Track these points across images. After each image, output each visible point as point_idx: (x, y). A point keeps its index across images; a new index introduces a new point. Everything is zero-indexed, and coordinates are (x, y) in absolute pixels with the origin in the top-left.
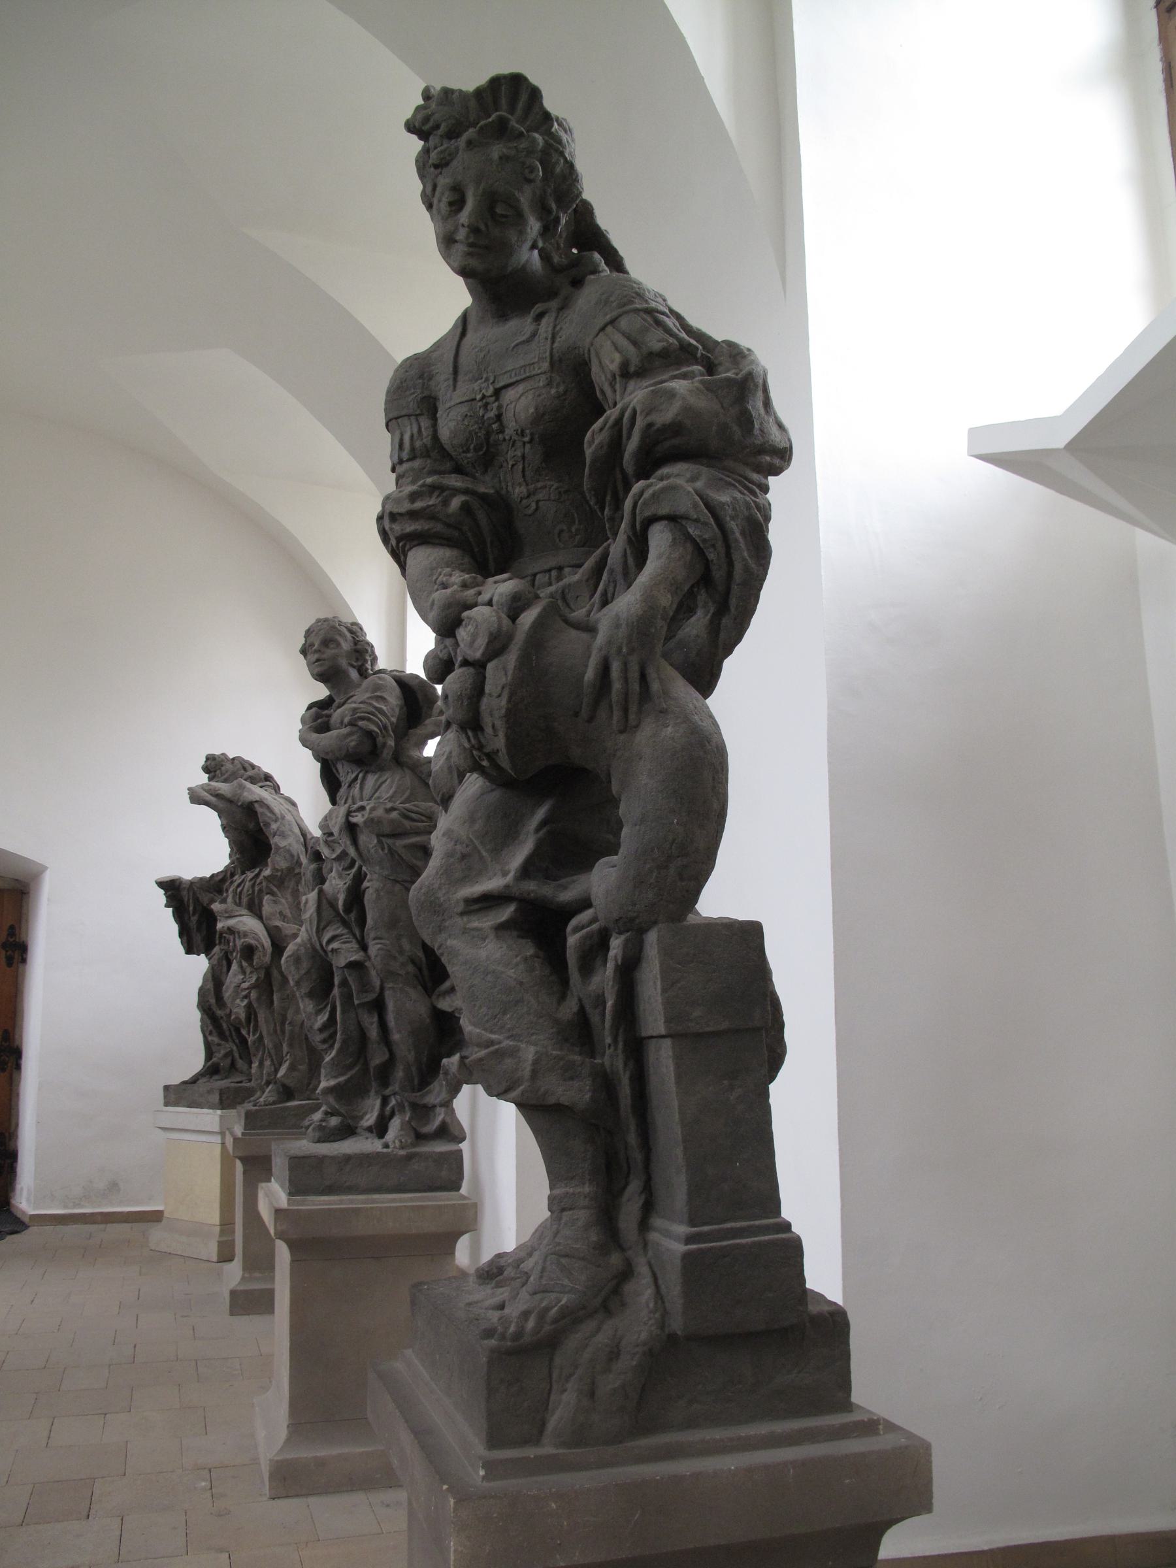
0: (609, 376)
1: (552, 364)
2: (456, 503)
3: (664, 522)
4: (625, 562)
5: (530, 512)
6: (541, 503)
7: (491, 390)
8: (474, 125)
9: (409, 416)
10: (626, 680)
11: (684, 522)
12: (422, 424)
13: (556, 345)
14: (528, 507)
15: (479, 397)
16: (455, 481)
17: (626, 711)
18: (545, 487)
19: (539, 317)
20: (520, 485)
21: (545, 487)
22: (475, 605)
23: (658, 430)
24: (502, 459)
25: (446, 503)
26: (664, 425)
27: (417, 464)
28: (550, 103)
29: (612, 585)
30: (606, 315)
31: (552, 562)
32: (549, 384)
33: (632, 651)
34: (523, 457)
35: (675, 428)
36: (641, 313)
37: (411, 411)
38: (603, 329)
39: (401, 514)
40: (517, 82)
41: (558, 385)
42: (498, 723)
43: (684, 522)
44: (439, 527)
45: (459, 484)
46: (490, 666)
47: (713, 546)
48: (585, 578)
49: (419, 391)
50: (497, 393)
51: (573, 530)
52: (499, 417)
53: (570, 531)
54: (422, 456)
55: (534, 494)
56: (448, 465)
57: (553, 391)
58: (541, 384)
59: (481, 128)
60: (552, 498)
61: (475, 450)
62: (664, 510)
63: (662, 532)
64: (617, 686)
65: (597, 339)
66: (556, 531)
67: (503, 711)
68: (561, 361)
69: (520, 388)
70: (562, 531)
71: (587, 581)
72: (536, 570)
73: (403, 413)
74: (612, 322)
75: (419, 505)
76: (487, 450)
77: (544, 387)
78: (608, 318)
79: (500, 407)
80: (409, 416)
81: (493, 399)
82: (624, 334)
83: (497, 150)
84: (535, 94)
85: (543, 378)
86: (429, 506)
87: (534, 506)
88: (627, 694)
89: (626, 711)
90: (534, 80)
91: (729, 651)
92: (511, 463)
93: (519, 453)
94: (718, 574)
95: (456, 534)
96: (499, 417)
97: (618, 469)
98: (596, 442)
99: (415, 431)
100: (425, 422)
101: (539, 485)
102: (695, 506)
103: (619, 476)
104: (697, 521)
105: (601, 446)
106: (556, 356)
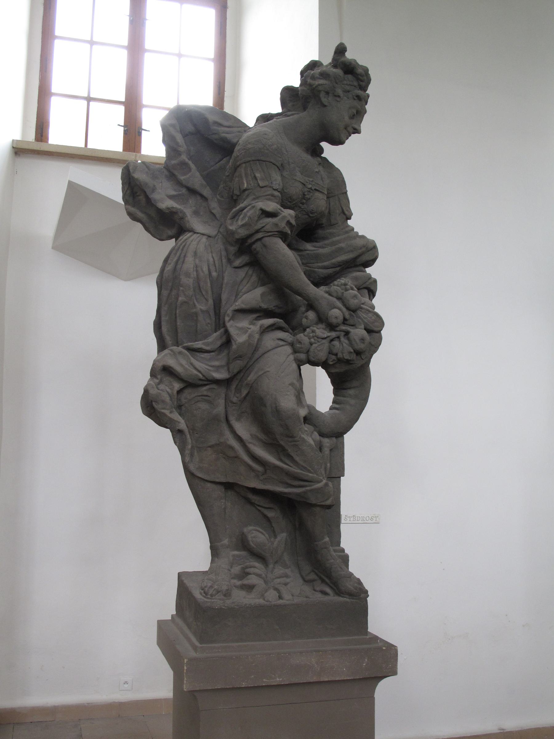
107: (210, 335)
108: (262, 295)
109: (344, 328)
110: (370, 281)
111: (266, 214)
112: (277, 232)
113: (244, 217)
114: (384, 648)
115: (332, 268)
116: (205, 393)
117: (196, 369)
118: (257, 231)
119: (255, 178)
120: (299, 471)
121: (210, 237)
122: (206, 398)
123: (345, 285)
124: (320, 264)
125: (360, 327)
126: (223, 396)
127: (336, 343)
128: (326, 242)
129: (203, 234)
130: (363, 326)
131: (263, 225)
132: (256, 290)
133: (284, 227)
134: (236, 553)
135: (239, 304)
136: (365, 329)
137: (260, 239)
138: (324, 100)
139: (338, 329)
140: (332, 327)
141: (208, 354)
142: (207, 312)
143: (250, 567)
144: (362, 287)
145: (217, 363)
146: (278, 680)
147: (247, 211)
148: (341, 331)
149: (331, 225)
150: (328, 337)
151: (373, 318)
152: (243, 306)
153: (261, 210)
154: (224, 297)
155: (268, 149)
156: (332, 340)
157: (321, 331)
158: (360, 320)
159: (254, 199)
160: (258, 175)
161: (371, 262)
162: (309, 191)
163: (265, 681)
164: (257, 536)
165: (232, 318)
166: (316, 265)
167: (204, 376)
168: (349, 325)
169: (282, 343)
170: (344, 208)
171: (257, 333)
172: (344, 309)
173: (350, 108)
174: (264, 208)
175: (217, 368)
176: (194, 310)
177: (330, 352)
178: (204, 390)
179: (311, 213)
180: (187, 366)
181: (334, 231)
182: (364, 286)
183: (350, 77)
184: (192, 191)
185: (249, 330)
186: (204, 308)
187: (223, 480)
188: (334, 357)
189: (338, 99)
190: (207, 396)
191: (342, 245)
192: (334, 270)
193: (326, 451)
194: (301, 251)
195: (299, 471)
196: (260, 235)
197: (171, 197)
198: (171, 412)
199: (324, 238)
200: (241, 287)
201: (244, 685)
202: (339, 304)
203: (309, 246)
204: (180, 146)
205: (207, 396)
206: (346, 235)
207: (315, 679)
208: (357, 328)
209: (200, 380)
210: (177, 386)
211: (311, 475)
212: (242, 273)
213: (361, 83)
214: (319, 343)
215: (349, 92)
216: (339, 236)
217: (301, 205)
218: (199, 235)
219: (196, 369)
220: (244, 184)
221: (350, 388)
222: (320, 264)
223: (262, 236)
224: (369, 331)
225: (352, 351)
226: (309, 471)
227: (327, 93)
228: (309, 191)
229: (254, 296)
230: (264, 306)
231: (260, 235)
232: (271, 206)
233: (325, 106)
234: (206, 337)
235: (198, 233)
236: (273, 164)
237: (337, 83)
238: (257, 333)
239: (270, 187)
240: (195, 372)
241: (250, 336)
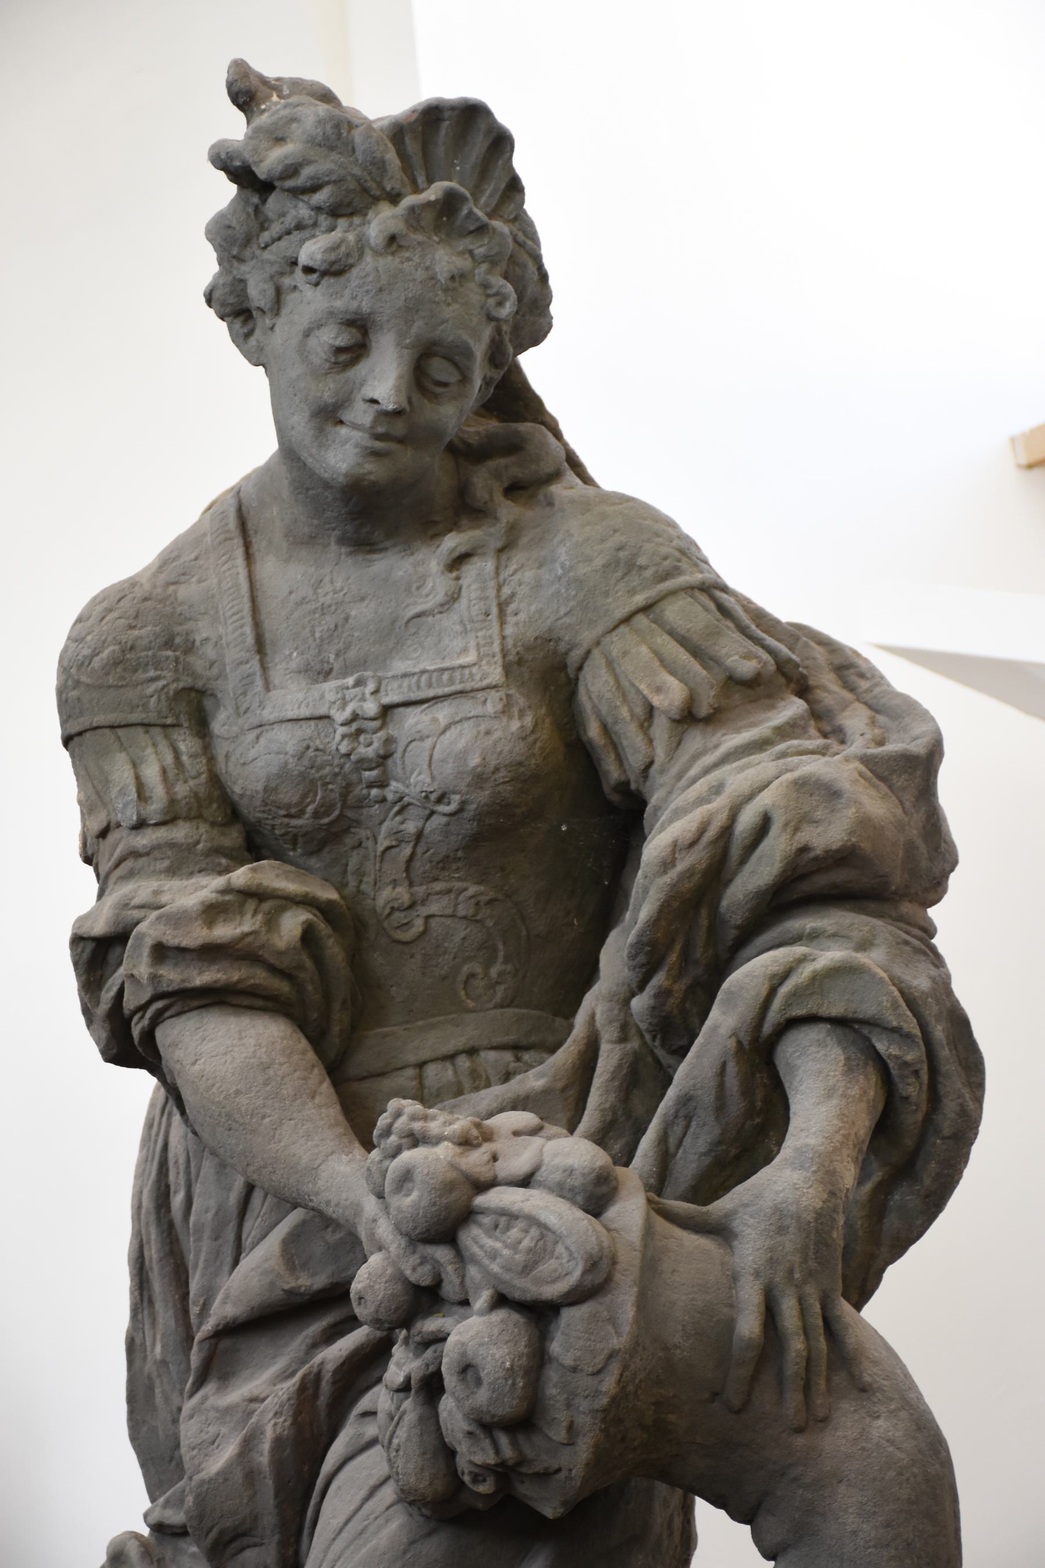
0: (639, 710)
1: (507, 669)
2: (292, 924)
3: (826, 1027)
4: (721, 1086)
5: (400, 935)
6: (433, 922)
7: (371, 708)
8: (394, 198)
9: (146, 726)
10: (806, 1331)
11: (865, 1031)
12: (182, 747)
13: (509, 630)
14: (408, 925)
15: (340, 716)
16: (270, 875)
17: (807, 1389)
18: (449, 891)
19: (458, 561)
20: (395, 883)
21: (449, 891)
22: (493, 1183)
23: (816, 859)
24: (363, 833)
25: (271, 922)
26: (827, 852)
27: (180, 833)
28: (521, 162)
29: (681, 1122)
30: (632, 592)
31: (457, 1041)
32: (506, 710)
33: (811, 1274)
34: (419, 835)
35: (844, 857)
36: (697, 593)
37: (152, 717)
38: (627, 620)
39: (182, 950)
40: (472, 113)
41: (521, 715)
42: (583, 1420)
43: (865, 1031)
44: (260, 977)
45: (291, 886)
46: (570, 1316)
47: (916, 1073)
48: (560, 1085)
49: (169, 675)
50: (386, 711)
51: (494, 972)
52: (384, 758)
53: (486, 974)
54: (188, 818)
55: (424, 902)
56: (233, 838)
57: (515, 725)
58: (490, 709)
59: (412, 210)
60: (461, 911)
61: (316, 815)
62: (836, 1008)
63: (821, 1044)
64: (796, 1345)
65: (614, 637)
66: (462, 977)
67: (605, 1401)
68: (520, 662)
69: (443, 713)
70: (472, 976)
71: (564, 1090)
72: (425, 1054)
73: (135, 717)
74: (646, 609)
75: (224, 931)
76: (341, 815)
77: (496, 717)
78: (640, 599)
79: (389, 741)
80: (146, 726)
81: (376, 724)
82: (672, 633)
83: (445, 259)
84: (501, 142)
85: (494, 695)
86: (246, 935)
87: (419, 925)
88: (809, 1360)
89: (807, 1389)
90: (503, 116)
91: (899, 1249)
92: (383, 843)
93: (411, 827)
94: (912, 1119)
95: (283, 987)
96: (384, 758)
97: (704, 912)
98: (680, 867)
99: (169, 759)
100: (187, 744)
101: (438, 886)
102: (895, 1006)
103: (704, 922)
104: (895, 1030)
105: (689, 873)
106: (512, 657)
173: (307, 334)
182: (774, 1016)
217: (374, 792)
228: (359, 732)
237: (240, 259)
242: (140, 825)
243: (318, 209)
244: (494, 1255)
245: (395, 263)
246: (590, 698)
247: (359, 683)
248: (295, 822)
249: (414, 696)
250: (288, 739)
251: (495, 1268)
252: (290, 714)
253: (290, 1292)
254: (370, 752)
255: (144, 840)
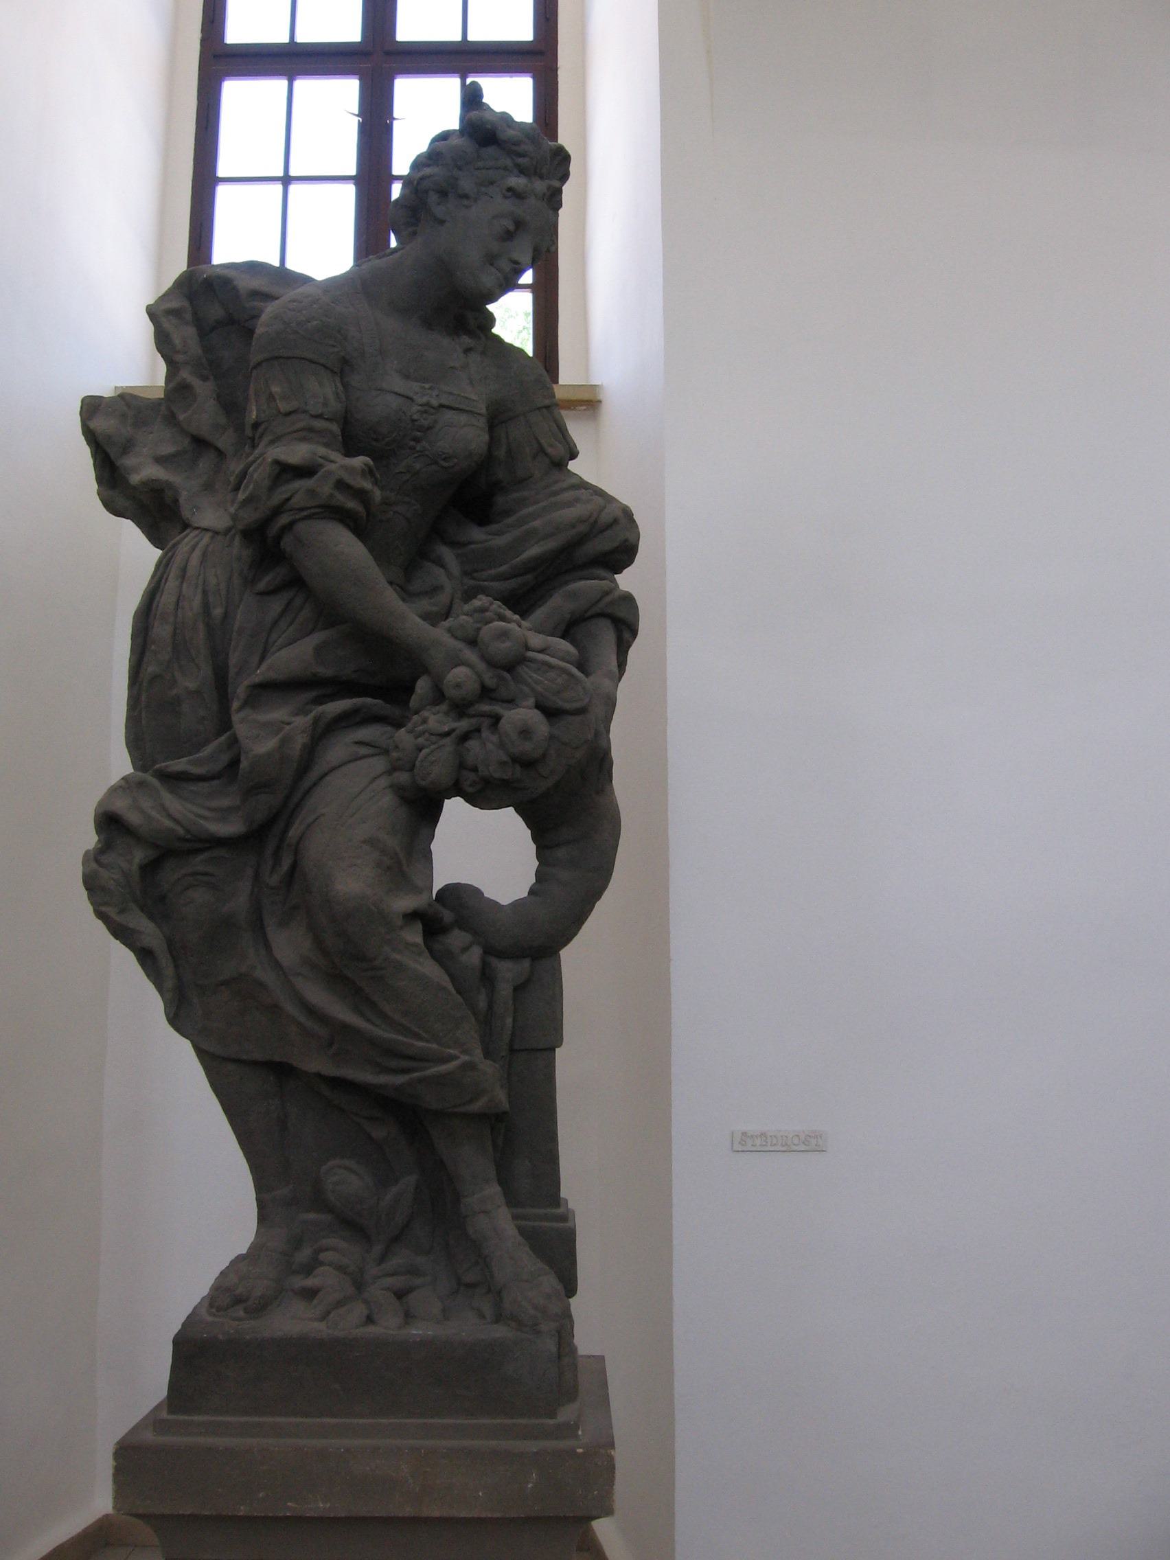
9: (326, 368)
19: (468, 351)
52: (430, 428)
69: (463, 418)
73: (322, 361)
96: (430, 428)
101: (407, 499)
107: (207, 742)
108: (318, 650)
109: (486, 707)
110: (608, 599)
111: (286, 471)
112: (319, 506)
113: (247, 487)
114: (580, 1450)
115: (516, 576)
116: (201, 868)
117: (170, 816)
118: (277, 511)
119: (271, 397)
120: (394, 1036)
121: (216, 533)
122: (206, 878)
123: (483, 610)
124: (493, 572)
125: (525, 703)
126: (250, 872)
127: (473, 744)
128: (510, 520)
129: (206, 530)
130: (531, 701)
131: (285, 496)
132: (307, 639)
133: (331, 495)
134: (312, 1216)
135: (261, 674)
136: (538, 706)
137: (290, 526)
138: (439, 211)
139: (471, 711)
140: (460, 709)
141: (206, 784)
142: (198, 693)
143: (327, 1250)
144: (589, 614)
145: (225, 802)
146: (320, 1506)
147: (255, 470)
148: (482, 716)
149: (522, 482)
150: (453, 730)
151: (559, 680)
152: (273, 675)
153: (277, 462)
154: (234, 659)
155: (296, 332)
156: (465, 737)
157: (436, 719)
158: (525, 688)
159: (272, 442)
160: (276, 389)
161: (624, 554)
162: (425, 412)
163: (291, 1507)
164: (347, 1179)
165: (245, 704)
166: (485, 574)
167: (188, 831)
168: (503, 701)
169: (363, 751)
170: (542, 441)
171: (303, 732)
172: (481, 666)
173: (494, 217)
174: (283, 457)
175: (224, 814)
176: (174, 692)
177: (462, 766)
178: (198, 863)
179: (444, 459)
180: (154, 813)
181: (526, 493)
182: (596, 610)
183: (491, 150)
184: (200, 443)
185: (288, 727)
186: (192, 685)
187: (258, 1056)
188: (472, 776)
189: (466, 202)
190: (205, 874)
191: (536, 523)
192: (520, 580)
193: (505, 991)
194: (465, 545)
195: (394, 1036)
196: (284, 520)
197: (160, 460)
198: (122, 911)
199: (507, 513)
200: (274, 636)
201: (243, 1510)
202: (470, 655)
203: (477, 534)
204: (178, 352)
205: (205, 874)
206: (553, 499)
207: (408, 1511)
208: (518, 706)
209: (181, 839)
210: (139, 856)
211: (421, 1044)
212: (276, 605)
213: (520, 160)
214: (433, 747)
215: (492, 183)
216: (536, 503)
217: (412, 443)
218: (197, 532)
219: (170, 816)
220: (251, 412)
221: (558, 845)
222: (493, 572)
223: (291, 518)
224: (551, 713)
225: (505, 758)
226: (417, 1036)
227: (443, 194)
228: (425, 412)
229: (295, 655)
230: (326, 672)
231: (284, 520)
232: (297, 453)
233: (442, 222)
234: (200, 746)
235: (198, 528)
236: (312, 361)
237: (460, 169)
238: (303, 732)
239: (305, 412)
240: (168, 823)
241: (284, 742)
242: (319, 416)
243: (517, 166)
244: (537, 682)
245: (483, 205)
246: (507, 438)
247: (430, 388)
248: (374, 443)
249: (453, 405)
250: (395, 402)
251: (539, 688)
252: (396, 390)
253: (314, 675)
254: (426, 423)
255: (319, 424)
